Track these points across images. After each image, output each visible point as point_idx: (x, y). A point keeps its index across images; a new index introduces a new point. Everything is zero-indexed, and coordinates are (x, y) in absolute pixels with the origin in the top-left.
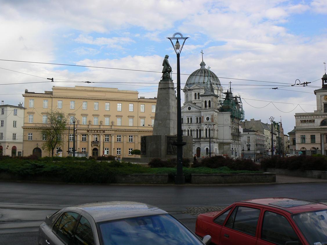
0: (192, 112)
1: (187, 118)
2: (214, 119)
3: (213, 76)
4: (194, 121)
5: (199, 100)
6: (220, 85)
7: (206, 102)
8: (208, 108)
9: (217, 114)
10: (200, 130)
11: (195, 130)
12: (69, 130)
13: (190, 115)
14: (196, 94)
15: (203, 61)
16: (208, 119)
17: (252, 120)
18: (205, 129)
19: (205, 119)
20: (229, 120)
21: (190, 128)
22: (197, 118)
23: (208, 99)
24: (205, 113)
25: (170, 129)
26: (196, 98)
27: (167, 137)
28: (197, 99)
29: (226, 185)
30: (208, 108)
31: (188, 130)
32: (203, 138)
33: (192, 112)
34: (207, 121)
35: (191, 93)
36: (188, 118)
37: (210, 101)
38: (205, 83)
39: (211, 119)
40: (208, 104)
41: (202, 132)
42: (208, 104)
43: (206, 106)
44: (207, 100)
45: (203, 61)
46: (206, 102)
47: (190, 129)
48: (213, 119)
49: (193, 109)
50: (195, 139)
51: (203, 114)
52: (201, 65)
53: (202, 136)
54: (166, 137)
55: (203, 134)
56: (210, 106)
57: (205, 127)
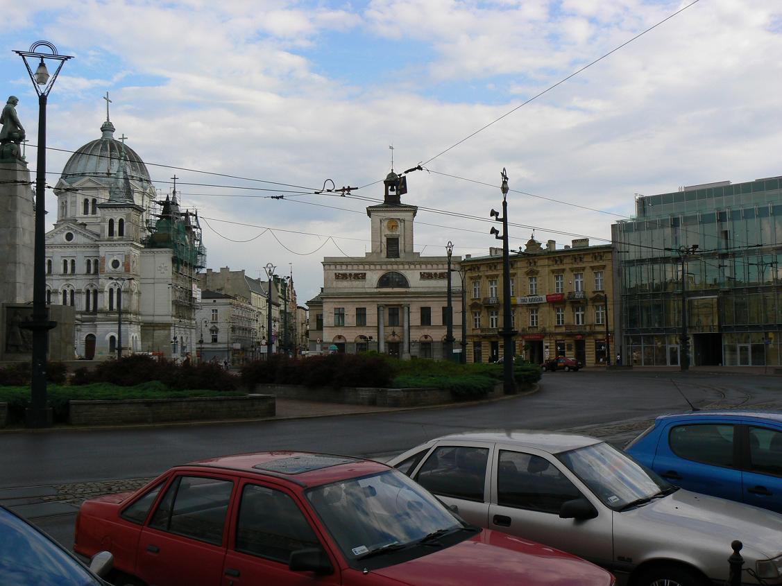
0: (76, 246)
1: (62, 261)
2: (131, 264)
3: (132, 158)
4: (81, 267)
5: (94, 216)
6: (149, 181)
7: (111, 222)
8: (116, 237)
9: (138, 252)
10: (96, 292)
11: (60, 290)
12: (704, 235)
13: (69, 252)
14: (86, 200)
15: (108, 120)
16: (115, 264)
17: (225, 270)
18: (107, 289)
19: (109, 266)
20: (168, 268)
21: (68, 286)
22: (89, 261)
23: (117, 215)
24: (108, 249)
25: (15, 287)
26: (86, 212)
27: (7, 307)
28: (90, 215)
29: (156, 425)
30: (116, 237)
31: (65, 292)
32: (102, 312)
33: (76, 246)
34: (113, 269)
35: (74, 199)
36: (65, 262)
37: (121, 222)
38: (111, 174)
39: (123, 265)
40: (116, 228)
41: (99, 295)
42: (116, 228)
43: (111, 233)
44: (116, 217)
45: (108, 120)
46: (111, 222)
47: (71, 288)
48: (128, 265)
49: (77, 239)
50: (82, 313)
51: (103, 251)
52: (103, 129)
53: (100, 306)
54: (5, 309)
55: (104, 302)
56: (121, 233)
57: (107, 285)
